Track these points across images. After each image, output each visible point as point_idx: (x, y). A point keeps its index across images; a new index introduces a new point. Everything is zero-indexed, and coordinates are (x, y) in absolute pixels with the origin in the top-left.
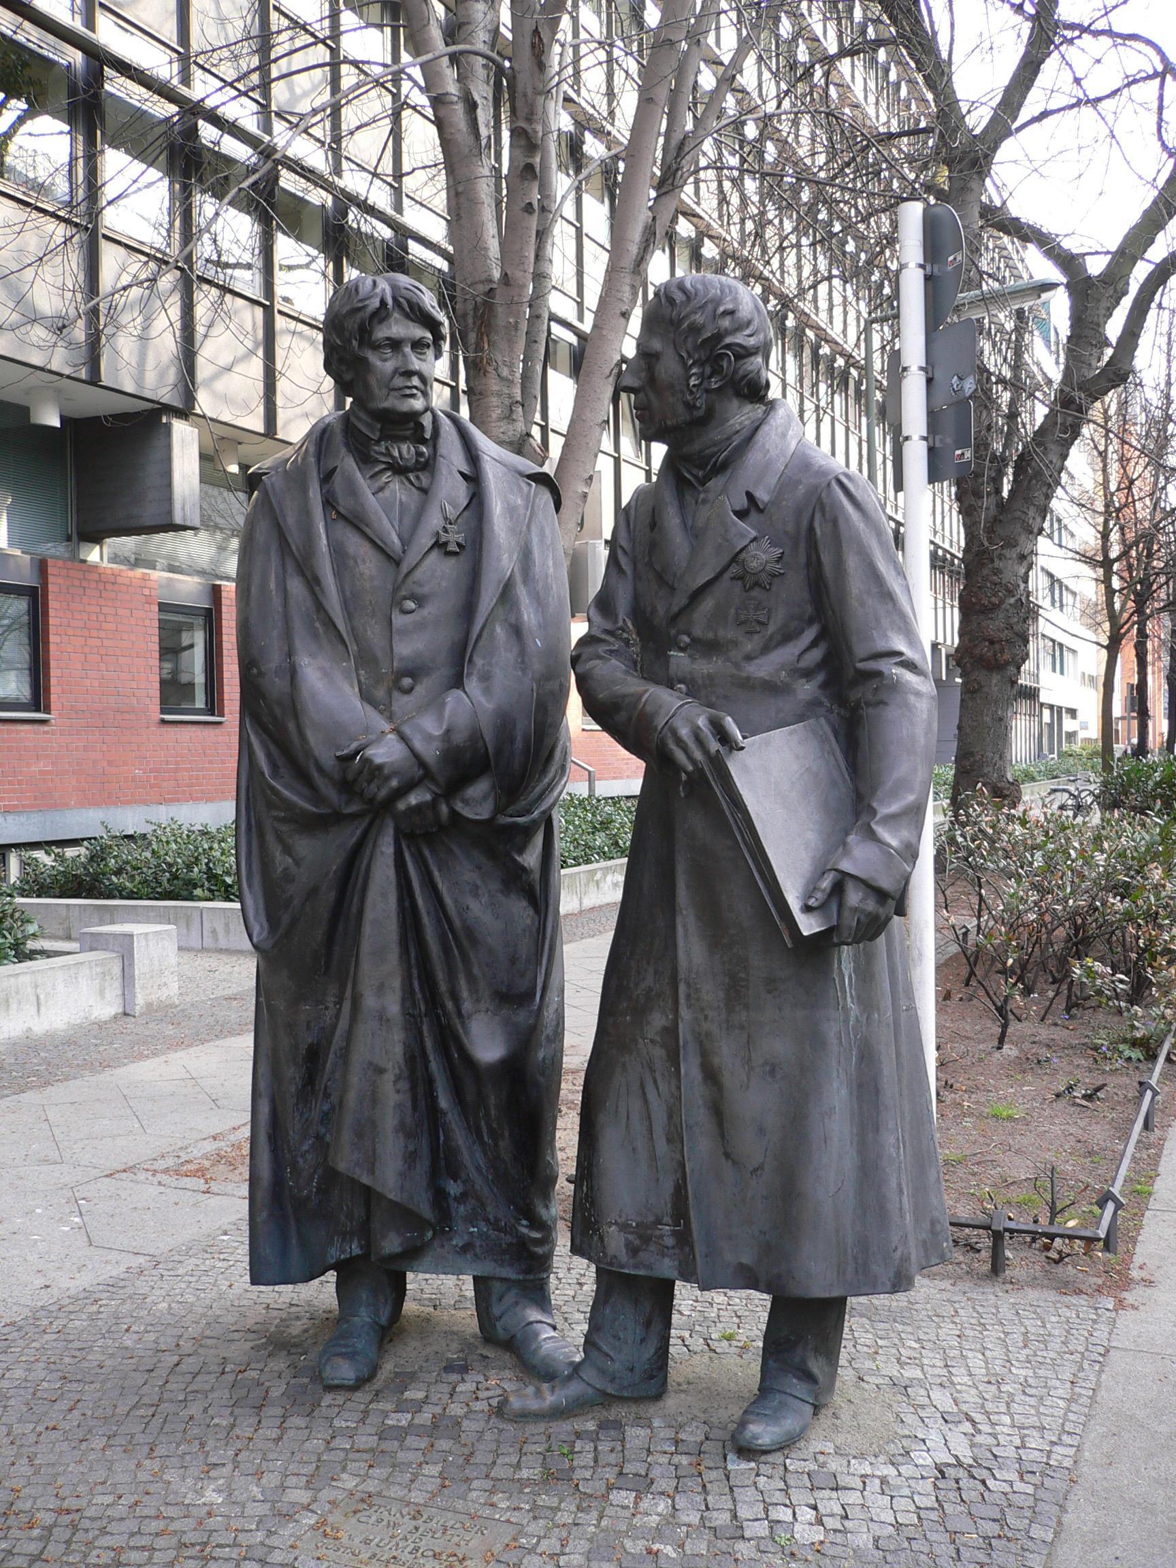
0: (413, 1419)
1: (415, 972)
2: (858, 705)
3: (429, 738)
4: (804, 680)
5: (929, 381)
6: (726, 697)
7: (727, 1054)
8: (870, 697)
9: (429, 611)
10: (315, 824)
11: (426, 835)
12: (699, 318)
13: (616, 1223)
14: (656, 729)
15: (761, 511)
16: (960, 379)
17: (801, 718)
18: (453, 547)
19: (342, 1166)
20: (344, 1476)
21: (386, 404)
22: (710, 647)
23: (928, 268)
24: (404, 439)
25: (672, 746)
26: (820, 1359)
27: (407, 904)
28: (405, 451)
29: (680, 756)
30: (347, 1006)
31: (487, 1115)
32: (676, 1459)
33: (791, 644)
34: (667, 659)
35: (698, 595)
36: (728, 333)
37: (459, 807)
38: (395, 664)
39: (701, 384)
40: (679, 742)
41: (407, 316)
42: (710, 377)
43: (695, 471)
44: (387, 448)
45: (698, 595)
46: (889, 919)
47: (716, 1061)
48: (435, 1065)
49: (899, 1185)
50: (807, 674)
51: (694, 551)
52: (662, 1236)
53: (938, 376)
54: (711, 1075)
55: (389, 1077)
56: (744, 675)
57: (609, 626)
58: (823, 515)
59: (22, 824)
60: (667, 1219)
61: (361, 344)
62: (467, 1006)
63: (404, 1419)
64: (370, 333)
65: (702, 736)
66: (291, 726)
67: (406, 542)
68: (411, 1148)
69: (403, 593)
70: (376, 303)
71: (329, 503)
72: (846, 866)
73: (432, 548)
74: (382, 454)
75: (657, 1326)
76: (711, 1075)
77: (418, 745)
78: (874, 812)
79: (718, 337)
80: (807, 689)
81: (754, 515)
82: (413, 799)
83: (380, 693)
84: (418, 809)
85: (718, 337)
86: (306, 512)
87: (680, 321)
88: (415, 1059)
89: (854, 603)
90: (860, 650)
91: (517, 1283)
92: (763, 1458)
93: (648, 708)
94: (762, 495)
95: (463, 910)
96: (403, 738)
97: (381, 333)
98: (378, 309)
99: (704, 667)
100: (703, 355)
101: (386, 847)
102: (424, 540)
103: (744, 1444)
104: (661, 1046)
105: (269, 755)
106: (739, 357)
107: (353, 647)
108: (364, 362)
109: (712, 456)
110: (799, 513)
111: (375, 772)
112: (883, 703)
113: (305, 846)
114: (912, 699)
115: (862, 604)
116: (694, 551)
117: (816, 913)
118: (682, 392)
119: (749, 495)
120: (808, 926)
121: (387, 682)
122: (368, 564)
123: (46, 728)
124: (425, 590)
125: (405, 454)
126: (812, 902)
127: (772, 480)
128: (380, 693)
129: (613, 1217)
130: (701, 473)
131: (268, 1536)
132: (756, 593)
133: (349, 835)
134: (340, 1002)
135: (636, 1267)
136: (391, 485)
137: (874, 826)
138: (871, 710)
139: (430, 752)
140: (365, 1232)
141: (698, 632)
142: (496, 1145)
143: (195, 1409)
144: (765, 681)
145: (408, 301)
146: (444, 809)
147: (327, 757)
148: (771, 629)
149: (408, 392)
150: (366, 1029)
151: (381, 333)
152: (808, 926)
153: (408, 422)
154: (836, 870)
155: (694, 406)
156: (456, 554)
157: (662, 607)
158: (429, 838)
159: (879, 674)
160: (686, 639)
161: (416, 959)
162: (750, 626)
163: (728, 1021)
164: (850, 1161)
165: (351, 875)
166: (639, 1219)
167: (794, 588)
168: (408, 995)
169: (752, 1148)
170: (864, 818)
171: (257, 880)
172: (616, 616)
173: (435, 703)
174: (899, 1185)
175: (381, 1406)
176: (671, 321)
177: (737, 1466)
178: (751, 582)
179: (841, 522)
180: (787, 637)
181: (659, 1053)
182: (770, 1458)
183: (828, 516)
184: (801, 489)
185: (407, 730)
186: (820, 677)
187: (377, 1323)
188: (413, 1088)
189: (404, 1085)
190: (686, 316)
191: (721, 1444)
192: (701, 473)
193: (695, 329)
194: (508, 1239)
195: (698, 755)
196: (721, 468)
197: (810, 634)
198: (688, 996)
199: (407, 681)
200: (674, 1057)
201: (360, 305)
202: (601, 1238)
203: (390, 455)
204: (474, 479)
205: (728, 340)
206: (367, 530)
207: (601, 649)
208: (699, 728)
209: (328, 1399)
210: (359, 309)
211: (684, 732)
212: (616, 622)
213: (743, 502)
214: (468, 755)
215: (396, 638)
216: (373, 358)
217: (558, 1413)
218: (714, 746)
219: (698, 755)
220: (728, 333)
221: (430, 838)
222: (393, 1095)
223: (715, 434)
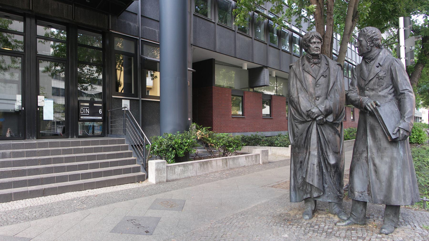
2: (400, 99)
3: (322, 108)
5: (405, 48)
7: (377, 161)
9: (321, 87)
10: (302, 122)
11: (321, 124)
12: (369, 34)
19: (307, 181)
22: (373, 90)
25: (367, 106)
28: (316, 61)
29: (368, 108)
30: (308, 154)
34: (365, 93)
37: (327, 119)
40: (368, 105)
48: (323, 164)
50: (390, 94)
51: (369, 74)
53: (407, 47)
54: (374, 165)
55: (315, 166)
76: (374, 165)
77: (320, 109)
80: (390, 97)
82: (319, 118)
84: (320, 120)
88: (319, 163)
90: (400, 89)
95: (328, 137)
99: (371, 93)
101: (315, 126)
102: (320, 75)
105: (294, 111)
108: (309, 46)
110: (388, 66)
111: (313, 113)
113: (300, 126)
116: (369, 74)
119: (379, 64)
124: (320, 83)
129: (356, 190)
132: (381, 80)
133: (308, 124)
134: (306, 153)
139: (322, 110)
140: (311, 193)
141: (370, 87)
146: (325, 120)
147: (305, 111)
148: (384, 86)
157: (363, 83)
158: (322, 125)
162: (379, 86)
165: (308, 131)
167: (387, 81)
168: (318, 153)
169: (384, 178)
170: (403, 118)
171: (291, 133)
173: (322, 103)
178: (379, 78)
181: (364, 161)
186: (393, 94)
188: (320, 168)
189: (318, 167)
193: (368, 36)
195: (372, 108)
196: (373, 60)
197: (391, 87)
199: (317, 99)
200: (367, 162)
211: (369, 104)
213: (378, 65)
216: (311, 45)
219: (372, 108)
222: (316, 168)
223: (372, 54)
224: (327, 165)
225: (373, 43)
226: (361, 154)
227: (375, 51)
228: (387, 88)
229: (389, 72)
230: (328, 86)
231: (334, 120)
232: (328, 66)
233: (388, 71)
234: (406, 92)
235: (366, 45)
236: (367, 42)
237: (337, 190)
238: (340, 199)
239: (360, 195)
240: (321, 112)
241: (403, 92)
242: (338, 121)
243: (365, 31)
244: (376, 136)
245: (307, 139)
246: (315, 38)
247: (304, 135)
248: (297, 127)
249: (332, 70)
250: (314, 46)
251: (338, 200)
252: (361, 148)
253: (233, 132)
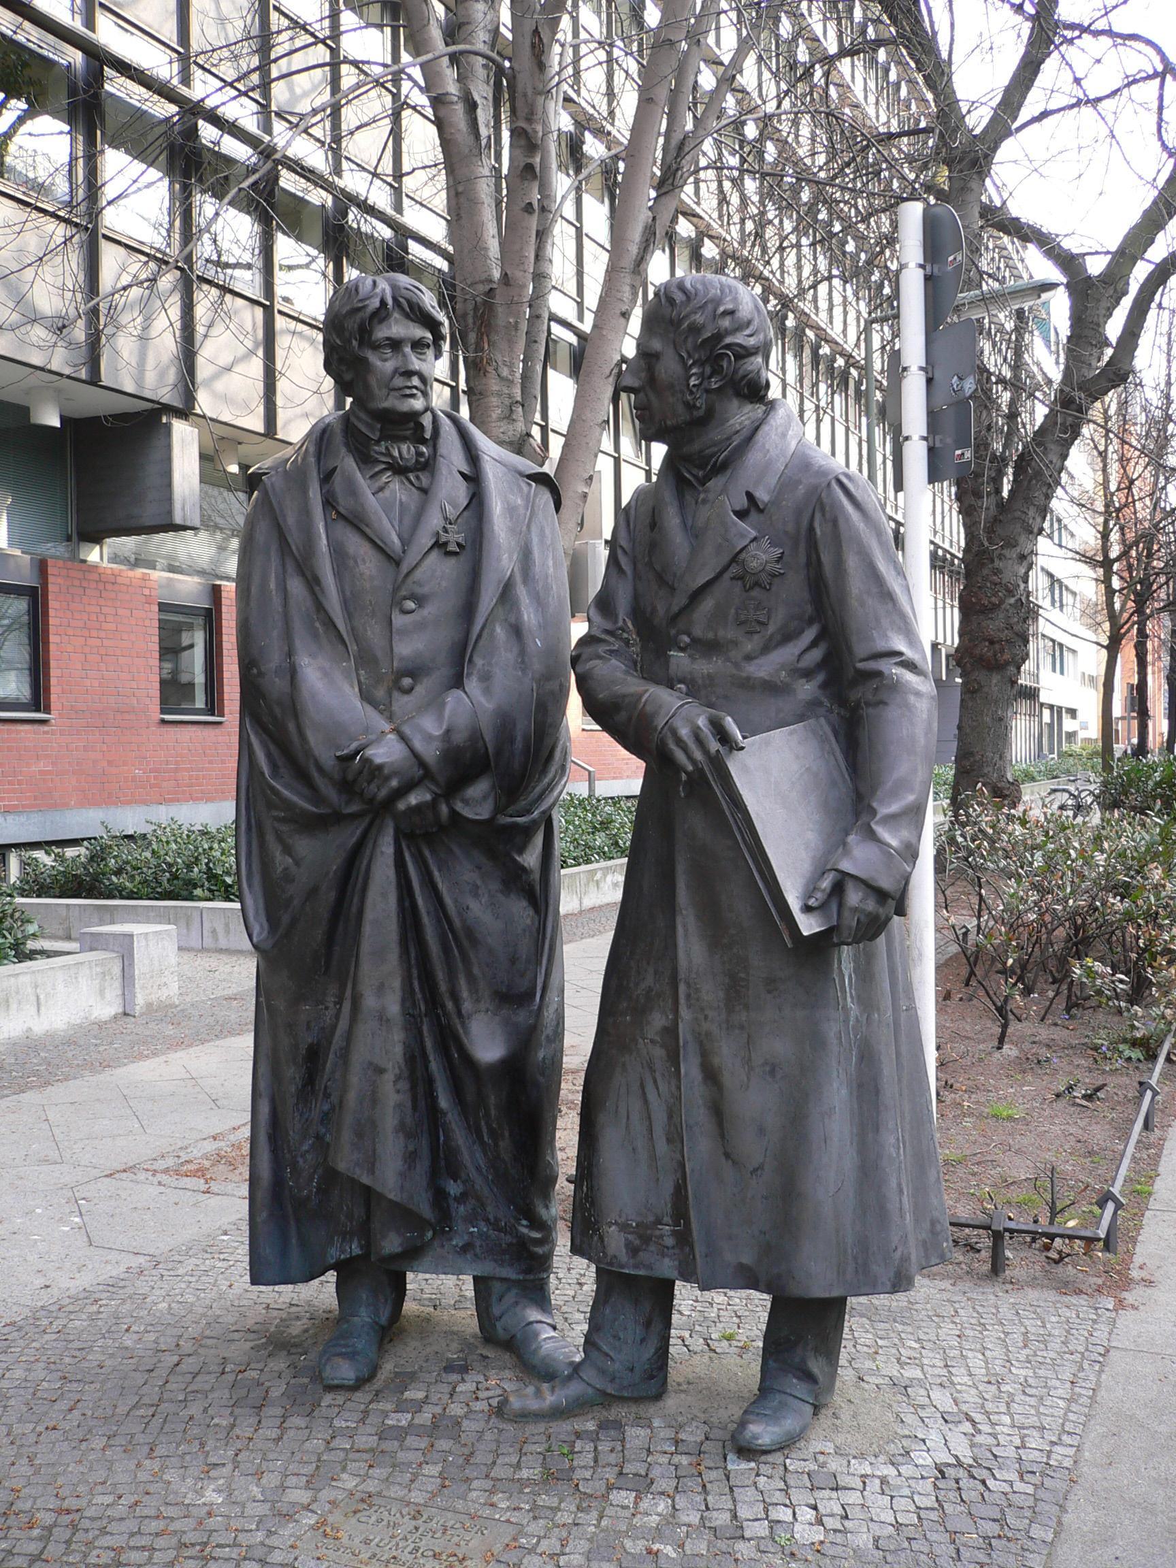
1: (415, 972)
2: (858, 705)
3: (429, 738)
4: (804, 680)
5: (929, 381)
6: (726, 697)
7: (727, 1054)
8: (870, 697)
9: (429, 611)
11: (426, 835)
12: (699, 318)
13: (616, 1223)
14: (656, 729)
15: (761, 511)
16: (960, 379)
17: (801, 718)
18: (453, 547)
19: (342, 1166)
20: (344, 1476)
21: (386, 404)
22: (710, 647)
23: (928, 268)
24: (404, 439)
25: (672, 746)
26: (820, 1359)
27: (407, 904)
28: (405, 451)
29: (680, 756)
30: (347, 1006)
31: (487, 1115)
32: (676, 1459)
33: (791, 644)
34: (667, 659)
35: (698, 595)
36: (728, 333)
37: (459, 807)
38: (395, 664)
39: (701, 384)
40: (679, 742)
41: (407, 316)
42: (710, 377)
43: (695, 471)
44: (387, 448)
45: (698, 595)
46: (889, 919)
48: (435, 1065)
49: (899, 1185)
50: (807, 674)
51: (694, 551)
52: (662, 1236)
53: (938, 376)
54: (711, 1075)
55: (389, 1077)
56: (744, 675)
57: (609, 626)
58: (823, 515)
59: (22, 824)
60: (667, 1219)
61: (361, 344)
62: (467, 1006)
63: (404, 1419)
64: (370, 333)
65: (702, 736)
66: (291, 726)
67: (406, 542)
68: (411, 1148)
69: (403, 593)
70: (376, 303)
71: (329, 503)
72: (846, 866)
73: (432, 548)
74: (382, 454)
75: (657, 1326)
76: (711, 1075)
77: (418, 745)
78: (874, 812)
79: (718, 337)
80: (807, 689)
81: (754, 515)
82: (413, 799)
83: (380, 693)
84: (418, 809)
85: (718, 337)
86: (306, 512)
87: (680, 321)
88: (415, 1059)
89: (854, 603)
90: (860, 650)
91: (517, 1283)
92: (763, 1458)
93: (648, 708)
94: (762, 495)
95: (463, 910)
96: (403, 738)
97: (381, 333)
98: (378, 309)
99: (704, 667)
100: (703, 355)
101: (386, 846)
102: (424, 540)
104: (661, 1046)
105: (269, 755)
106: (739, 357)
107: (353, 647)
108: (364, 362)
109: (712, 456)
110: (799, 513)
111: (375, 772)
112: (883, 703)
113: (305, 846)
114: (912, 699)
115: (862, 604)
116: (694, 551)
117: (816, 913)
118: (682, 392)
119: (749, 495)
120: (808, 926)
121: (387, 682)
122: (368, 564)
123: (46, 728)
124: (425, 590)
125: (405, 454)
126: (812, 902)
127: (772, 480)
128: (380, 693)
129: (613, 1217)
130: (701, 473)
131: (268, 1536)
132: (756, 593)
133: (349, 835)
134: (340, 1002)
135: (636, 1267)
136: (391, 485)
137: (874, 826)
138: (871, 710)
139: (430, 752)
140: (365, 1232)
141: (698, 632)
142: (496, 1145)
143: (195, 1409)
144: (765, 681)
145: (408, 301)
146: (444, 809)
147: (326, 757)
148: (771, 629)
149: (408, 392)
150: (366, 1029)
151: (381, 333)
152: (808, 926)
153: (408, 422)
154: (836, 870)
155: (694, 406)
156: (456, 554)
157: (662, 607)
158: (429, 838)
159: (879, 674)
160: (686, 639)
161: (416, 959)
162: (750, 626)
163: (728, 1021)
164: (850, 1161)
165: (351, 875)
166: (639, 1219)
167: (794, 588)
168: (408, 995)
169: (752, 1148)
170: (864, 818)
172: (616, 616)
173: (435, 703)
174: (899, 1185)
175: (381, 1406)
176: (671, 321)
177: (737, 1466)
178: (751, 582)
179: (841, 522)
180: (787, 637)
181: (659, 1053)
182: (770, 1458)
183: (828, 516)
184: (801, 489)
185: (407, 730)
186: (820, 677)
187: (377, 1323)
188: (413, 1088)
189: (404, 1085)
190: (686, 316)
192: (701, 473)
193: (695, 329)
194: (509, 1239)
195: (698, 755)
196: (721, 468)
197: (810, 634)
198: (688, 996)
199: (407, 681)
200: (674, 1057)
201: (360, 305)
202: (601, 1238)
203: (390, 455)
204: (474, 479)
205: (728, 340)
206: (367, 530)
207: (601, 649)
208: (699, 728)
209: (328, 1399)
210: (359, 309)
211: (684, 732)
212: (616, 622)
213: (743, 502)
214: (468, 755)
215: (396, 638)
216: (373, 358)
217: (558, 1413)
218: (714, 746)
219: (698, 755)
220: (728, 333)
221: (430, 838)
222: (393, 1095)
223: (715, 434)
231: (499, 810)
250: (389, 366)
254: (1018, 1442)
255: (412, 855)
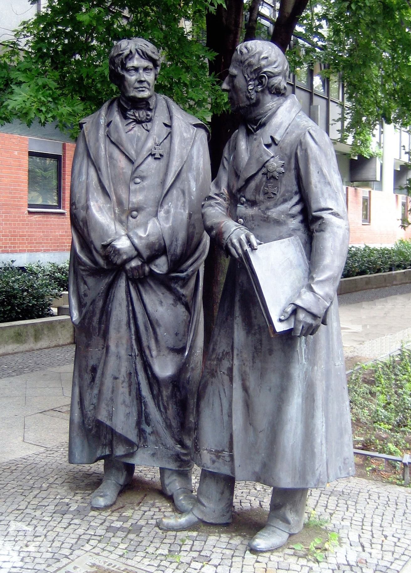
0: (324, 543)
1: (134, 337)
3: (140, 238)
4: (292, 219)
6: (258, 225)
9: (145, 183)
13: (206, 449)
14: (224, 239)
15: (276, 145)
17: (290, 235)
18: (157, 156)
20: (87, 545)
21: (132, 94)
22: (253, 203)
24: (141, 109)
25: (230, 247)
26: (292, 514)
27: (131, 308)
28: (141, 114)
29: (233, 251)
31: (162, 399)
32: (225, 551)
33: (286, 203)
35: (248, 181)
36: (265, 67)
38: (130, 206)
39: (253, 89)
40: (233, 245)
41: (141, 57)
42: (258, 85)
45: (248, 181)
46: (317, 327)
47: (248, 384)
49: (321, 442)
50: (293, 216)
52: (224, 457)
57: (217, 192)
58: (301, 147)
59: (51, 257)
60: (227, 449)
61: (122, 69)
62: (154, 353)
63: (118, 524)
64: (125, 64)
65: (242, 243)
66: (85, 230)
67: (138, 154)
68: (127, 412)
69: (135, 175)
71: (108, 136)
72: (299, 303)
73: (149, 156)
75: (227, 493)
76: (245, 389)
77: (136, 241)
79: (260, 69)
81: (273, 146)
85: (260, 69)
86: (97, 140)
87: (244, 62)
88: (132, 374)
89: (313, 186)
90: (314, 206)
91: (176, 471)
92: (260, 554)
94: (277, 138)
96: (129, 238)
97: (130, 64)
98: (129, 55)
100: (254, 76)
102: (145, 153)
103: (253, 548)
104: (227, 375)
106: (269, 77)
107: (114, 198)
111: (117, 252)
112: (322, 231)
114: (336, 229)
115: (316, 187)
117: (285, 322)
118: (246, 92)
119: (272, 138)
120: (280, 327)
121: (127, 213)
122: (122, 162)
123: (63, 217)
125: (142, 116)
126: (282, 318)
127: (282, 131)
128: (124, 218)
130: (255, 127)
131: (47, 567)
135: (214, 468)
136: (135, 129)
137: (312, 285)
138: (318, 234)
142: (166, 412)
143: (38, 513)
144: (275, 219)
146: (147, 269)
147: (98, 244)
149: (141, 89)
150: (112, 361)
151: (130, 64)
152: (280, 327)
154: (293, 304)
155: (251, 98)
156: (159, 159)
159: (321, 218)
160: (244, 199)
161: (135, 332)
163: (253, 367)
164: (299, 430)
165: (108, 293)
166: (216, 448)
167: (289, 183)
172: (221, 189)
174: (321, 442)
175: (112, 518)
176: (241, 62)
177: (249, 555)
178: (271, 177)
179: (309, 151)
182: (265, 554)
183: (303, 148)
184: (294, 135)
185: (131, 234)
186: (300, 218)
187: (118, 483)
190: (247, 60)
191: (384, 559)
192: (255, 127)
194: (172, 452)
195: (240, 251)
197: (296, 199)
198: (238, 355)
199: (135, 213)
201: (121, 52)
202: (200, 455)
205: (265, 70)
207: (212, 202)
208: (241, 239)
209: (93, 513)
211: (235, 241)
213: (270, 141)
214: (157, 246)
215: (131, 194)
216: (127, 75)
217: (182, 529)
218: (246, 247)
219: (240, 251)
220: (265, 67)
224: (152, 380)
225: (261, 83)
226: (220, 360)
227: (270, 102)
228: (285, 201)
229: (293, 161)
230: (163, 182)
231: (170, 270)
232: (169, 129)
233: (290, 159)
234: (325, 214)
235: (244, 89)
236: (247, 82)
237: (176, 440)
238: (182, 460)
239: (214, 458)
240: (136, 249)
241: (318, 214)
242: (182, 272)
243: (245, 51)
244: (254, 320)
245: (106, 313)
246: (137, 56)
247: (100, 304)
248: (85, 283)
249: (176, 140)
251: (178, 464)
252: (222, 346)
253: (32, 251)
254: (380, 557)
255: (134, 288)
